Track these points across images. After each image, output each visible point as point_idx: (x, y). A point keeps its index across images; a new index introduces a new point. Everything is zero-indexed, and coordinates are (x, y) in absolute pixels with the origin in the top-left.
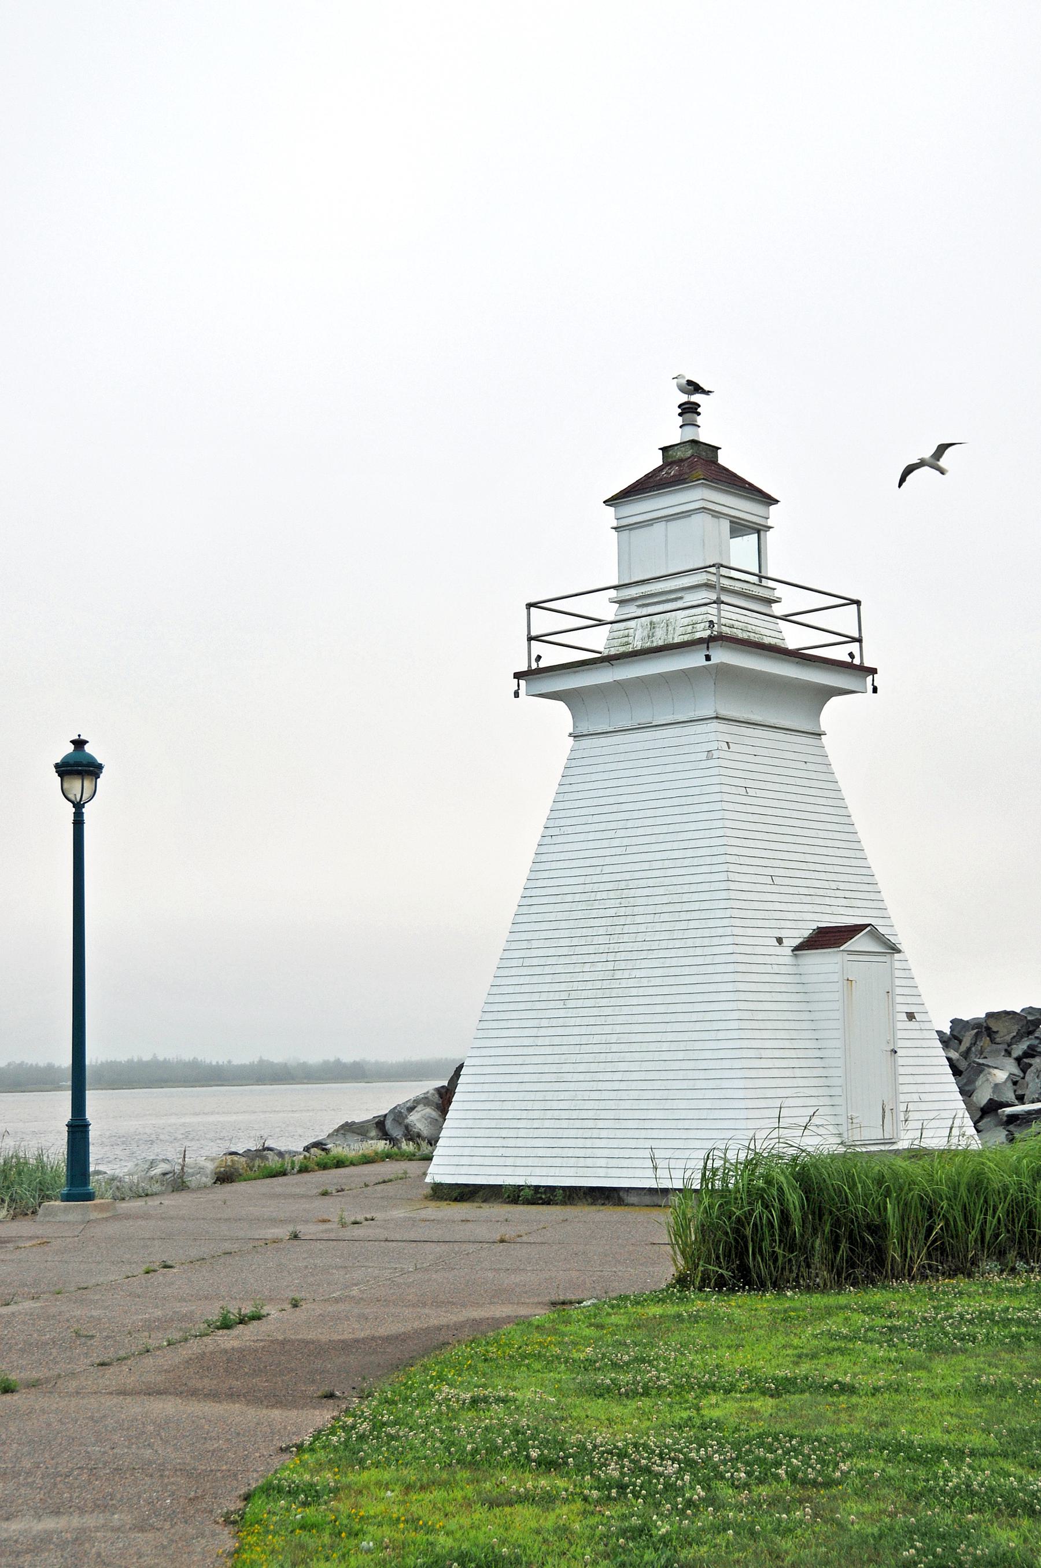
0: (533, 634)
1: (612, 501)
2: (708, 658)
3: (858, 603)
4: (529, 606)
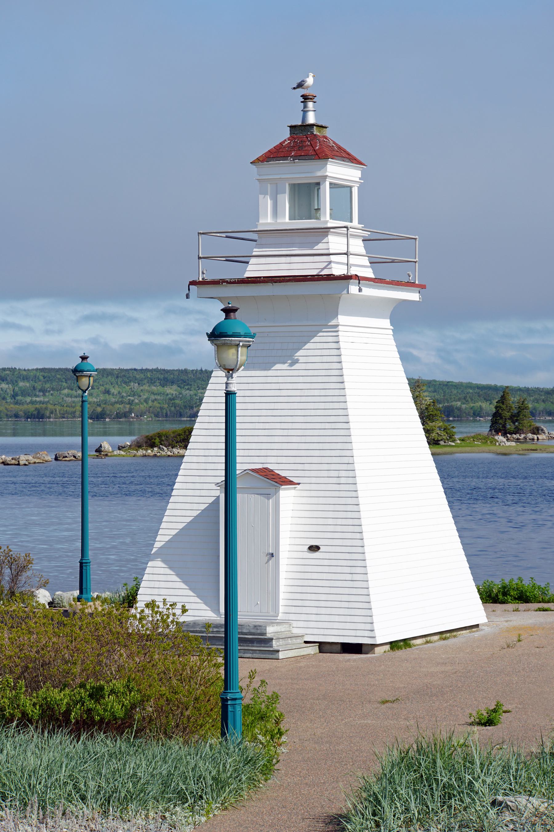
0: (200, 255)
2: (360, 290)
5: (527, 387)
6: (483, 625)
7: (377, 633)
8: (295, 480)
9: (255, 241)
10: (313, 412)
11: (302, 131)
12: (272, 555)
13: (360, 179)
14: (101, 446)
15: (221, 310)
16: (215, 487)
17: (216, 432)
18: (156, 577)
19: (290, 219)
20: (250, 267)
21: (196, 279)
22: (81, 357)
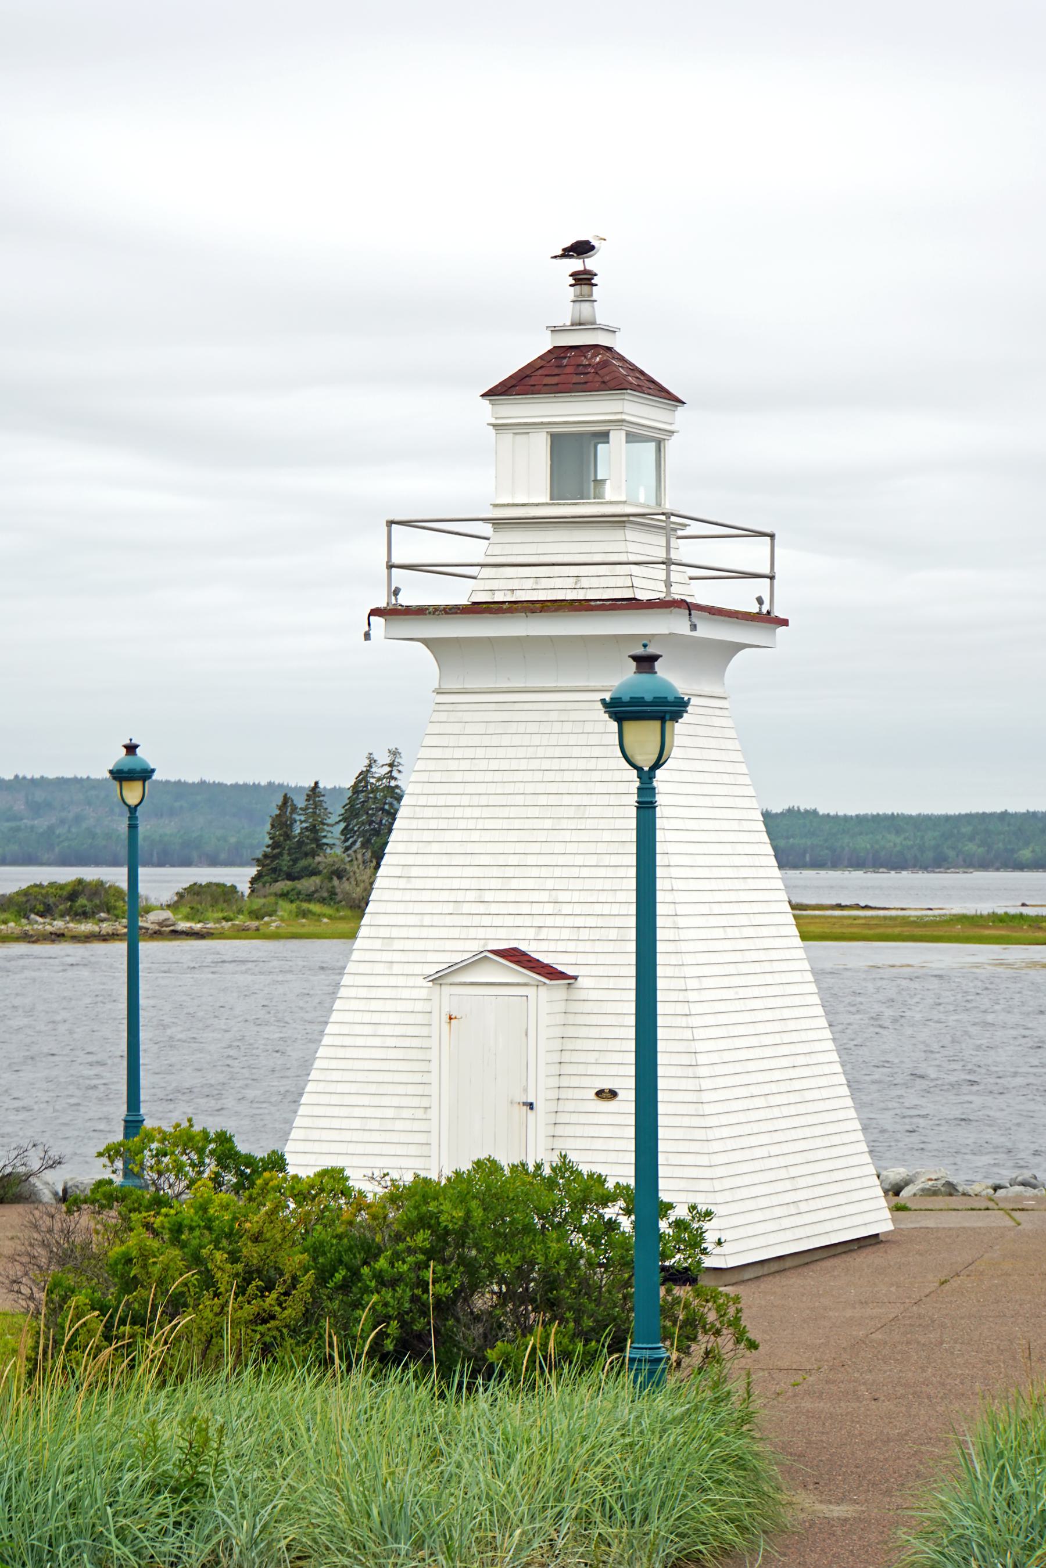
0: (395, 560)
2: (694, 627)
3: (772, 536)
4: (390, 523)
5: (1031, 810)
8: (570, 971)
9: (488, 539)
17: (621, 872)
21: (382, 604)
22: (125, 746)
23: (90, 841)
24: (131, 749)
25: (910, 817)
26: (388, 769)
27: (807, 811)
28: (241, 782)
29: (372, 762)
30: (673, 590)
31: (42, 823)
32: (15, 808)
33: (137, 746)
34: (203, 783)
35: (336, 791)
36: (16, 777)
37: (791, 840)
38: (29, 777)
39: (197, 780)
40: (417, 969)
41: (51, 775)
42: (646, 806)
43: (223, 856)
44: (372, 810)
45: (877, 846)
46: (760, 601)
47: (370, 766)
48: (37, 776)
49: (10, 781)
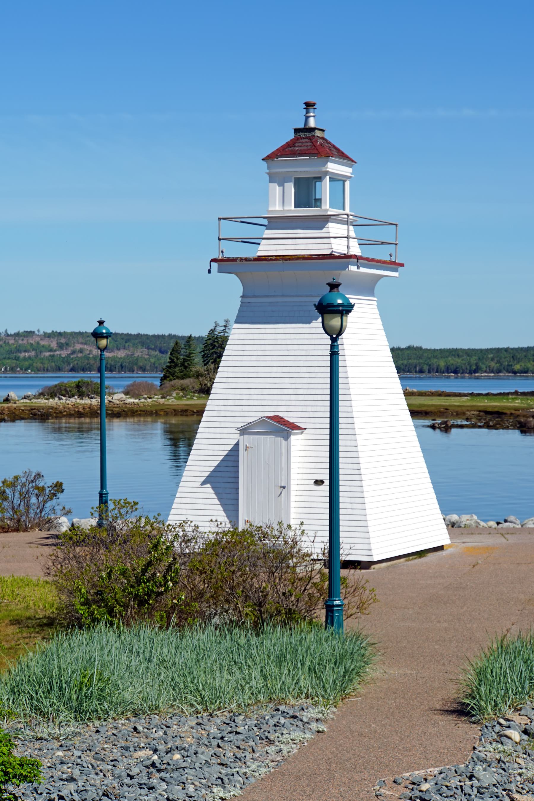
0: (220, 237)
1: (269, 158)
3: (396, 225)
4: (220, 219)
6: (449, 546)
7: (373, 552)
8: (302, 426)
10: (317, 370)
11: (305, 132)
12: (284, 487)
13: (351, 174)
14: (8, 396)
15: (328, 284)
16: (234, 431)
18: (183, 506)
19: (295, 207)
20: (260, 247)
21: (216, 256)
22: (98, 322)
23: (86, 361)
24: (101, 323)
25: (464, 350)
26: (223, 328)
27: (417, 347)
28: (156, 334)
29: (217, 325)
30: (350, 250)
31: (64, 353)
32: (52, 346)
33: (104, 322)
34: (139, 334)
35: (200, 339)
36: (53, 331)
37: (410, 361)
38: (58, 331)
39: (136, 333)
40: (233, 425)
41: (69, 330)
42: (334, 354)
43: (148, 368)
44: (214, 348)
45: (448, 364)
46: (391, 255)
47: (216, 327)
48: (62, 331)
49: (50, 333)
